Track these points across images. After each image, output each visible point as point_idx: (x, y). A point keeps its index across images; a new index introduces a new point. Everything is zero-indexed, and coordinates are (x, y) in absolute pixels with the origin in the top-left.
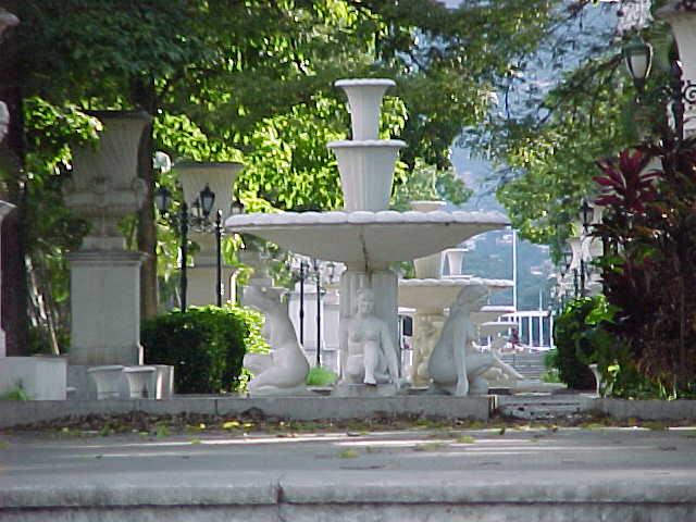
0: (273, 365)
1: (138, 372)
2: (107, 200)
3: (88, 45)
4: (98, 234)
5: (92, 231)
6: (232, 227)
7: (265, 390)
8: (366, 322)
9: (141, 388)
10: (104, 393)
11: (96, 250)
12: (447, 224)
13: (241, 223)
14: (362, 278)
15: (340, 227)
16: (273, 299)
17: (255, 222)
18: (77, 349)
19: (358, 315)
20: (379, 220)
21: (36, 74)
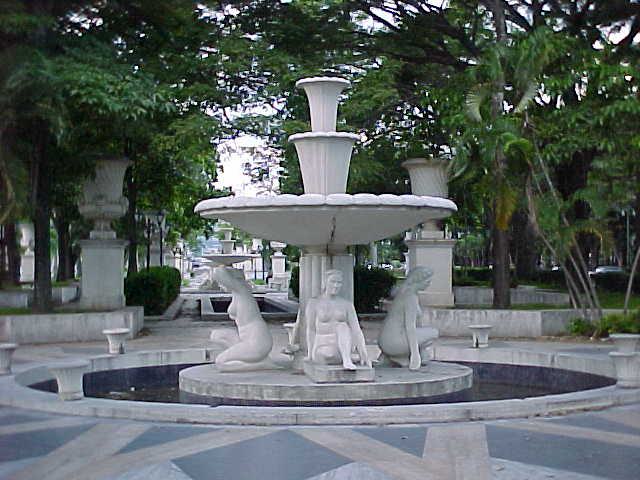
0: (240, 341)
1: (116, 334)
2: (104, 208)
3: (81, 87)
4: (99, 229)
5: (96, 227)
6: (203, 211)
7: (233, 365)
8: (333, 302)
9: (119, 346)
10: (65, 393)
11: (97, 238)
12: (419, 207)
13: (217, 206)
14: (324, 260)
15: (343, 209)
16: (239, 279)
17: (228, 206)
18: (86, 298)
19: (326, 295)
20: (357, 202)
21: (41, 105)
